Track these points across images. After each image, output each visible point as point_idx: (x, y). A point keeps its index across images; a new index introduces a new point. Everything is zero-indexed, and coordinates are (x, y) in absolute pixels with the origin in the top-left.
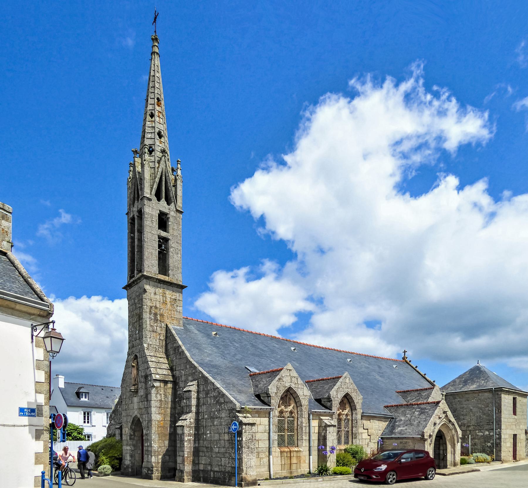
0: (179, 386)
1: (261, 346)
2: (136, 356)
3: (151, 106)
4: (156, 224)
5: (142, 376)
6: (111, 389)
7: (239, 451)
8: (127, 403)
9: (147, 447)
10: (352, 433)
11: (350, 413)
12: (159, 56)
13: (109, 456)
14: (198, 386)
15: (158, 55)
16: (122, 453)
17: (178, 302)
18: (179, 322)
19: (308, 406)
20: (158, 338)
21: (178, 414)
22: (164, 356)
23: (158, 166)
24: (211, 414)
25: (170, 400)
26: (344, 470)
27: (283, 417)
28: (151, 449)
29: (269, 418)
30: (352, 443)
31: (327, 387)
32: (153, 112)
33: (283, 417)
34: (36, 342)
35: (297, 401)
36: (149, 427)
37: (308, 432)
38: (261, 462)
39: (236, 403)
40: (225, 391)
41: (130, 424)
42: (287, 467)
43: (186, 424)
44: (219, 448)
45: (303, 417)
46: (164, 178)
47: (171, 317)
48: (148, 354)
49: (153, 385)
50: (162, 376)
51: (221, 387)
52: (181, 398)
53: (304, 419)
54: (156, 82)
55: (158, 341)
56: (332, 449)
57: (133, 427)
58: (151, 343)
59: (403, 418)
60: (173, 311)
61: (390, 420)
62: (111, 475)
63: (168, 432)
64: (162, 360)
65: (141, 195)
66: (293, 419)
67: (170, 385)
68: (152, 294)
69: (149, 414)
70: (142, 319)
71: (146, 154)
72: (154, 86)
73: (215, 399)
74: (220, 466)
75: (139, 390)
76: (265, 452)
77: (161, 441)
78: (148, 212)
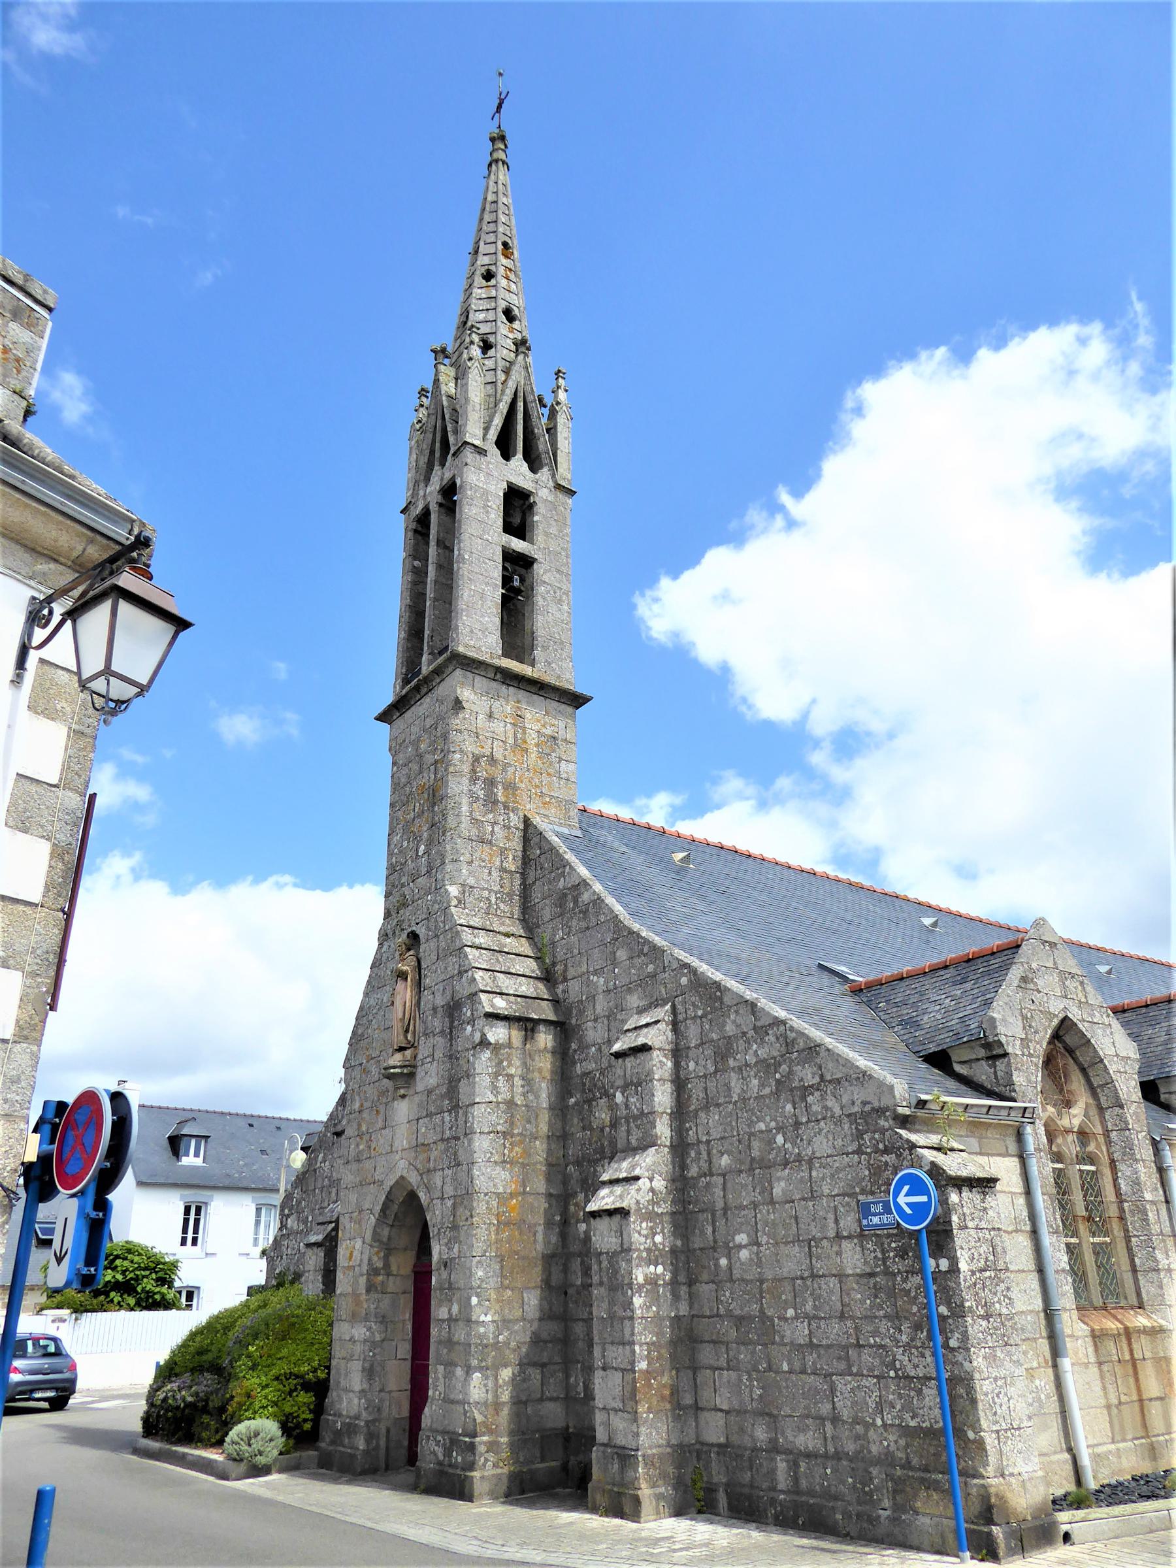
0: (580, 1040)
2: (414, 936)
4: (496, 518)
5: (435, 1009)
6: (277, 1123)
8: (364, 1128)
13: (274, 1371)
14: (675, 1025)
17: (563, 746)
18: (567, 810)
20: (498, 864)
21: (578, 1163)
23: (503, 379)
24: (749, 1147)
28: (468, 1334)
32: (493, 268)
34: (40, 688)
35: (1096, 1082)
41: (373, 1220)
42: (1130, 1414)
43: (638, 1202)
44: (810, 1318)
46: (520, 405)
47: (542, 795)
48: (462, 921)
49: (484, 1035)
50: (516, 1003)
52: (595, 1091)
55: (495, 874)
58: (471, 881)
60: (549, 774)
62: (280, 1471)
64: (510, 944)
66: (1093, 1168)
67: (545, 1039)
68: (481, 717)
73: (767, 1072)
74: (829, 1427)
75: (419, 1069)
76: (1035, 1339)
77: (509, 1293)
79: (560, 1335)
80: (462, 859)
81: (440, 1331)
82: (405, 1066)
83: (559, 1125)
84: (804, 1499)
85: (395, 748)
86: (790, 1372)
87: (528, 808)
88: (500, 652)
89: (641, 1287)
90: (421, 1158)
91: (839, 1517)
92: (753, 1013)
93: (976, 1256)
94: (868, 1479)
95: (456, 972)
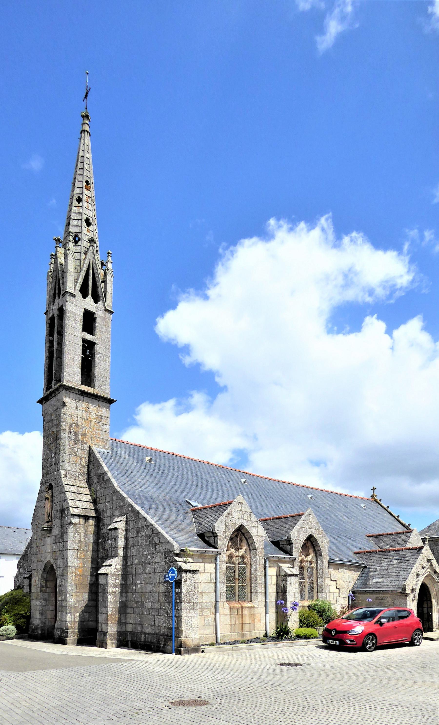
1: (205, 477)
2: (51, 486)
3: (78, 189)
5: (57, 510)
6: (25, 531)
7: (178, 606)
9: (61, 602)
10: (317, 585)
11: (314, 560)
12: (90, 135)
13: (13, 613)
14: (127, 522)
15: (89, 134)
16: (31, 609)
18: (106, 443)
19: (263, 549)
20: (79, 462)
21: (101, 559)
22: (86, 485)
23: (84, 257)
25: (92, 541)
26: (309, 633)
27: (233, 563)
28: (66, 604)
29: (215, 563)
30: (318, 598)
31: (286, 526)
32: (81, 196)
33: (233, 563)
35: (250, 543)
36: (64, 575)
37: (264, 582)
38: (205, 622)
39: (174, 543)
40: (160, 529)
41: (41, 572)
42: (238, 627)
43: (111, 572)
45: (258, 563)
46: (91, 271)
48: (65, 483)
49: (71, 521)
50: (82, 511)
51: (156, 524)
52: (106, 539)
53: (258, 567)
54: (85, 163)
55: (78, 466)
56: (294, 605)
57: (45, 576)
58: (69, 469)
59: (378, 568)
61: (362, 569)
62: (16, 639)
63: (89, 582)
64: (82, 491)
65: (63, 290)
66: (245, 566)
67: (92, 522)
69: (65, 558)
70: (59, 438)
71: (71, 243)
72: (82, 167)
73: (147, 538)
74: (153, 626)
75: (53, 529)
76: (210, 608)
78: (71, 310)
79: (95, 605)
80: (66, 461)
81: (59, 603)
82: (49, 528)
83: (96, 547)
84: (146, 643)
85: (45, 415)
86: (146, 615)
87: (91, 442)
88: (81, 383)
89: (110, 593)
90: (54, 555)
91: (153, 647)
92: (146, 521)
93: (188, 589)
94: (159, 639)
95: (63, 499)
